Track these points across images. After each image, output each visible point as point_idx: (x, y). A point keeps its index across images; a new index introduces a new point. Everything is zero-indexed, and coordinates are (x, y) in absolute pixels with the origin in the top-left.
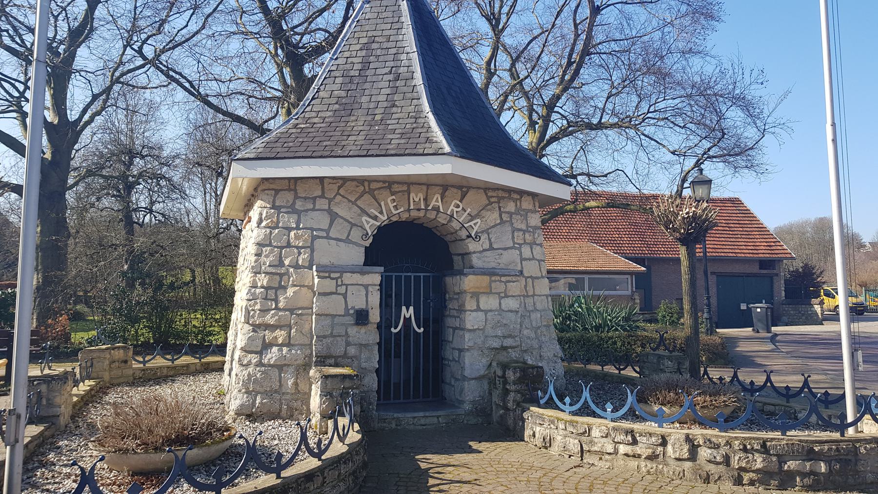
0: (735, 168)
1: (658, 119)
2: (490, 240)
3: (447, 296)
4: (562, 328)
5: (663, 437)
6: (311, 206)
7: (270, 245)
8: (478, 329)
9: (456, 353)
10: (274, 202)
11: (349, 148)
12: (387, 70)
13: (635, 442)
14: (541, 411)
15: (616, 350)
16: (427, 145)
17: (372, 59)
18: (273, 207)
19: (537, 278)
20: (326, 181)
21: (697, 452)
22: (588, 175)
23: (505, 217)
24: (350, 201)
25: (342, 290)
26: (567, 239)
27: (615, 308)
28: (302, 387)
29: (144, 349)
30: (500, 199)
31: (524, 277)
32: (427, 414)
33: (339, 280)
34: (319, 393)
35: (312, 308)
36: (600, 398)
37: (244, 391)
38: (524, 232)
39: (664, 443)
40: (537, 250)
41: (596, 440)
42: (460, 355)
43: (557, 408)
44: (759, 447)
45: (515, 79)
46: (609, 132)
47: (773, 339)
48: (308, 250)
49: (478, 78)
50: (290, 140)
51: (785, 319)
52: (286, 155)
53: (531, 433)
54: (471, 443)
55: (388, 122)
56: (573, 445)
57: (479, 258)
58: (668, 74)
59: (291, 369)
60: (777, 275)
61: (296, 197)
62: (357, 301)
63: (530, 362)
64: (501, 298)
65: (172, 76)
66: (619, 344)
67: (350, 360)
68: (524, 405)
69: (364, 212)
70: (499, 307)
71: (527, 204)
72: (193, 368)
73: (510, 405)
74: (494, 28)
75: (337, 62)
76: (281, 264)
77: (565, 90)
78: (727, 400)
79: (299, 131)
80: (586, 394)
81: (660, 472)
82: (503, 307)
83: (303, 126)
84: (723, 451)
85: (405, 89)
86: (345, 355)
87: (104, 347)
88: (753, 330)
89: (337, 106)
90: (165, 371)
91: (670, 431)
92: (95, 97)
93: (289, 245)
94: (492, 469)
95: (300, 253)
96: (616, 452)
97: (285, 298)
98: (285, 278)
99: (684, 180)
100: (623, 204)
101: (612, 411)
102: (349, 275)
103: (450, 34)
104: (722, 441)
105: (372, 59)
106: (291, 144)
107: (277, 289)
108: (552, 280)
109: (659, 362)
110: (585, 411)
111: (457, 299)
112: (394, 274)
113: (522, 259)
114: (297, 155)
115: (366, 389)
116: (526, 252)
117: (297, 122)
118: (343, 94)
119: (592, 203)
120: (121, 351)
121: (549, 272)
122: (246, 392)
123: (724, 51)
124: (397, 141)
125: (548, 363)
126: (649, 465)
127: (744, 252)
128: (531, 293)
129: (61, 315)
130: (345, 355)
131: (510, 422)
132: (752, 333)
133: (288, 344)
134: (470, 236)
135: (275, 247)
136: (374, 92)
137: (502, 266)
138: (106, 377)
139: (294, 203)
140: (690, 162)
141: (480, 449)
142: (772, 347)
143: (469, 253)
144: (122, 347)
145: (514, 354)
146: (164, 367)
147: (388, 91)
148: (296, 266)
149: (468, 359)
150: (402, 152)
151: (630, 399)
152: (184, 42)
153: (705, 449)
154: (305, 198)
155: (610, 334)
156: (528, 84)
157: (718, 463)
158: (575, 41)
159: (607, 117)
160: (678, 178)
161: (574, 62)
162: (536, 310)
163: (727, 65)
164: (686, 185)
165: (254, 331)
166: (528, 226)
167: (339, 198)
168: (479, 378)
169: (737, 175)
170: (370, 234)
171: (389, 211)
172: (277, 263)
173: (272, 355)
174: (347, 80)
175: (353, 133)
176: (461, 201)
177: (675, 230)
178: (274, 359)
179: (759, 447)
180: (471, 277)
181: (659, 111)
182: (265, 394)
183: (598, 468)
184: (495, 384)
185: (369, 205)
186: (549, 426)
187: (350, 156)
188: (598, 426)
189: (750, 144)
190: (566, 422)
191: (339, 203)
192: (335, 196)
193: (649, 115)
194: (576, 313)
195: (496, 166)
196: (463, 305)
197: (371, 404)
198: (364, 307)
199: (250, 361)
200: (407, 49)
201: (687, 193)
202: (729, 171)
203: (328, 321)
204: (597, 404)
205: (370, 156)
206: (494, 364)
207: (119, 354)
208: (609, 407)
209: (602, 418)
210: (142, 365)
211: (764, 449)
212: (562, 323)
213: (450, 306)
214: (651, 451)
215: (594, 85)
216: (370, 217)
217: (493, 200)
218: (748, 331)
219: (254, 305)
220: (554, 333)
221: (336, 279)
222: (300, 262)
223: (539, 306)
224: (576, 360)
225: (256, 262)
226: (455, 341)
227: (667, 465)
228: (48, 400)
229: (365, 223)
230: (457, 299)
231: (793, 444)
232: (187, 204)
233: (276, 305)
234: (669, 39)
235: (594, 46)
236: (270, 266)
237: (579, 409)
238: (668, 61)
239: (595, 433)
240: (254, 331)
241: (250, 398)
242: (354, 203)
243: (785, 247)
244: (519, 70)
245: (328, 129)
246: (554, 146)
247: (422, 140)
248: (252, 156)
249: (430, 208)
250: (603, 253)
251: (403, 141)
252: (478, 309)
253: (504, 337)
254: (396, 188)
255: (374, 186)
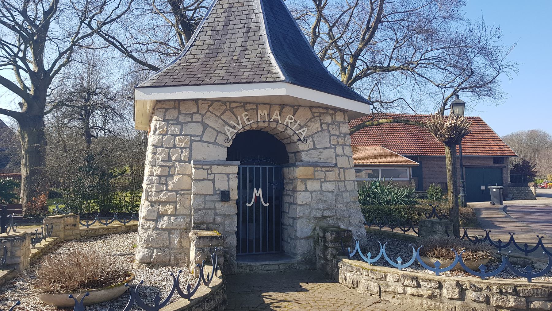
0: (479, 95)
1: (427, 64)
2: (314, 142)
3: (285, 181)
4: (364, 203)
5: (440, 283)
6: (190, 120)
7: (162, 146)
8: (306, 204)
9: (291, 220)
10: (164, 117)
11: (215, 79)
12: (242, 25)
13: (419, 286)
14: (350, 262)
15: (401, 217)
16: (269, 75)
17: (232, 18)
18: (164, 120)
19: (347, 169)
20: (200, 102)
21: (465, 294)
22: (381, 102)
23: (324, 127)
24: (216, 116)
25: (211, 177)
26: (367, 144)
27: (400, 188)
28: (185, 244)
29: (87, 217)
30: (321, 114)
31: (338, 168)
32: (271, 263)
33: (209, 170)
34: (195, 249)
35: (191, 190)
36: (392, 251)
37: (145, 246)
38: (338, 137)
39: (440, 287)
40: (347, 149)
41: (390, 284)
42: (293, 222)
43: (361, 259)
44: (511, 291)
45: (332, 39)
46: (396, 73)
47: (505, 209)
48: (188, 150)
49: (309, 39)
50: (175, 74)
51: (511, 196)
52: (172, 84)
53: (344, 277)
54: (301, 284)
55: (242, 61)
56: (374, 287)
57: (306, 155)
58: (435, 33)
59: (177, 232)
60: (505, 167)
61: (180, 113)
62: (222, 185)
63: (342, 227)
64: (322, 182)
65: (110, 40)
66: (403, 213)
67: (217, 226)
68: (338, 257)
69: (226, 123)
70: (323, 186)
71: (339, 117)
72: (120, 229)
73: (329, 257)
74: (318, 6)
75: (208, 21)
76: (170, 159)
77: (366, 44)
78: (485, 255)
79: (181, 68)
80: (383, 250)
81: (438, 308)
82: (324, 189)
83: (184, 64)
84: (484, 293)
85: (254, 38)
86: (214, 222)
87: (60, 216)
88: (491, 203)
89: (207, 51)
90: (101, 231)
91: (444, 278)
92: (61, 55)
93: (175, 146)
94: (316, 304)
95: (182, 152)
96: (405, 292)
97: (172, 183)
98: (172, 169)
99: (445, 104)
100: (404, 120)
101: (402, 263)
102: (216, 167)
103: (290, 9)
104: (484, 286)
105: (232, 18)
106: (175, 77)
107: (167, 177)
108: (357, 171)
109: (432, 226)
110: (382, 262)
111: (291, 183)
112: (248, 167)
113: (337, 156)
114: (179, 83)
115: (228, 246)
116: (339, 150)
117: (180, 62)
118: (212, 42)
119: (385, 120)
120: (72, 218)
121: (355, 166)
122: (147, 248)
123: (471, 18)
124: (248, 73)
125: (355, 227)
126: (429, 303)
127: (483, 151)
128: (343, 179)
129: (41, 195)
130: (214, 222)
131: (329, 269)
132: (490, 206)
133: (175, 214)
134: (300, 140)
135: (165, 148)
136: (233, 40)
137: (322, 160)
138: (62, 235)
139: (178, 118)
140: (451, 91)
141: (308, 288)
142: (504, 214)
143: (300, 152)
144: (72, 216)
145: (331, 221)
146: (101, 229)
147: (243, 40)
148: (180, 161)
149: (299, 224)
150: (251, 81)
151: (415, 255)
152: (117, 18)
153: (471, 292)
154: (186, 114)
155: (397, 207)
156: (340, 43)
157: (481, 302)
158: (372, 13)
159: (394, 62)
160: (441, 103)
161: (371, 28)
162: (346, 191)
163: (474, 26)
164: (446, 107)
165: (151, 205)
166: (340, 133)
167: (209, 113)
168: (307, 238)
169: (480, 100)
170: (230, 138)
171: (243, 122)
172: (167, 159)
173: (164, 222)
174: (215, 33)
175: (218, 68)
176: (293, 115)
177: (441, 136)
178: (165, 225)
179: (511, 291)
180: (300, 168)
181: (428, 59)
182: (160, 249)
183: (392, 304)
184: (318, 242)
185: (230, 118)
186: (355, 272)
187: (216, 84)
188: (392, 274)
189: (490, 79)
190: (368, 270)
191: (209, 118)
192: (206, 112)
193: (421, 62)
194: (374, 193)
195: (317, 90)
196: (295, 187)
197: (232, 256)
198: (227, 189)
199: (149, 226)
200: (256, 11)
201: (447, 113)
202: (475, 98)
203: (202, 199)
204: (389, 256)
205: (230, 83)
206: (317, 228)
207: (70, 220)
208: (400, 260)
209: (392, 267)
210: (86, 227)
211: (515, 292)
212: (364, 199)
213: (287, 188)
214: (430, 292)
215: (384, 40)
216: (231, 127)
217: (315, 114)
218: (487, 204)
219: (152, 188)
220: (358, 206)
221: (207, 169)
222: (182, 158)
223: (348, 188)
224: (374, 224)
225: (152, 158)
226: (290, 212)
227: (443, 303)
228: (12, 253)
229: (227, 131)
230: (291, 183)
231: (537, 289)
232: (127, 125)
233: (167, 188)
234: (435, 10)
235: (385, 16)
236: (162, 161)
237: (375, 263)
238: (434, 25)
239: (390, 278)
240: (151, 205)
241: (149, 251)
242: (219, 117)
243: (510, 149)
244: (334, 34)
245: (201, 66)
246: (358, 83)
247: (265, 72)
248: (148, 85)
249: (272, 120)
250: (390, 153)
251: (252, 73)
252: (306, 190)
253: (325, 210)
254: (248, 106)
255: (233, 105)
